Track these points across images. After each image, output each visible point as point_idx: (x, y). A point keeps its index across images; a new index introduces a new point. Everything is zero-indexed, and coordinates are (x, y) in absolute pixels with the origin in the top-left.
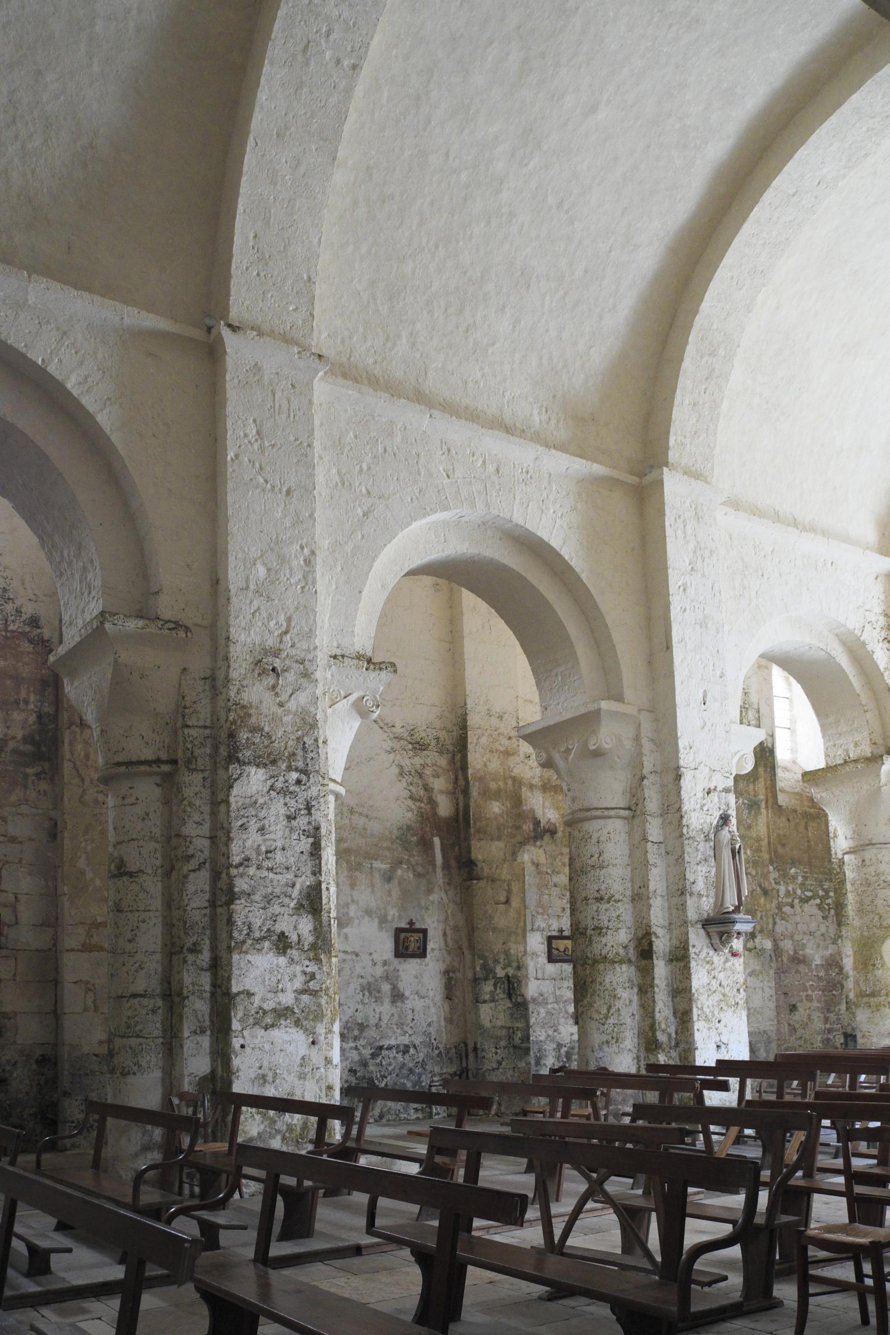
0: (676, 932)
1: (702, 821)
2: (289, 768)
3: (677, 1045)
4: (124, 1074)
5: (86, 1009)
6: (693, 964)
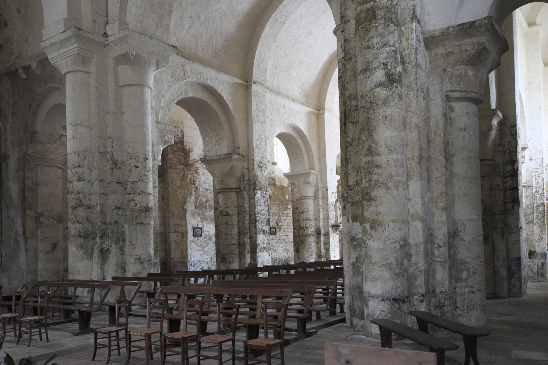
0: (326, 228)
2: (264, 191)
3: (325, 256)
5: (175, 249)
6: (330, 236)
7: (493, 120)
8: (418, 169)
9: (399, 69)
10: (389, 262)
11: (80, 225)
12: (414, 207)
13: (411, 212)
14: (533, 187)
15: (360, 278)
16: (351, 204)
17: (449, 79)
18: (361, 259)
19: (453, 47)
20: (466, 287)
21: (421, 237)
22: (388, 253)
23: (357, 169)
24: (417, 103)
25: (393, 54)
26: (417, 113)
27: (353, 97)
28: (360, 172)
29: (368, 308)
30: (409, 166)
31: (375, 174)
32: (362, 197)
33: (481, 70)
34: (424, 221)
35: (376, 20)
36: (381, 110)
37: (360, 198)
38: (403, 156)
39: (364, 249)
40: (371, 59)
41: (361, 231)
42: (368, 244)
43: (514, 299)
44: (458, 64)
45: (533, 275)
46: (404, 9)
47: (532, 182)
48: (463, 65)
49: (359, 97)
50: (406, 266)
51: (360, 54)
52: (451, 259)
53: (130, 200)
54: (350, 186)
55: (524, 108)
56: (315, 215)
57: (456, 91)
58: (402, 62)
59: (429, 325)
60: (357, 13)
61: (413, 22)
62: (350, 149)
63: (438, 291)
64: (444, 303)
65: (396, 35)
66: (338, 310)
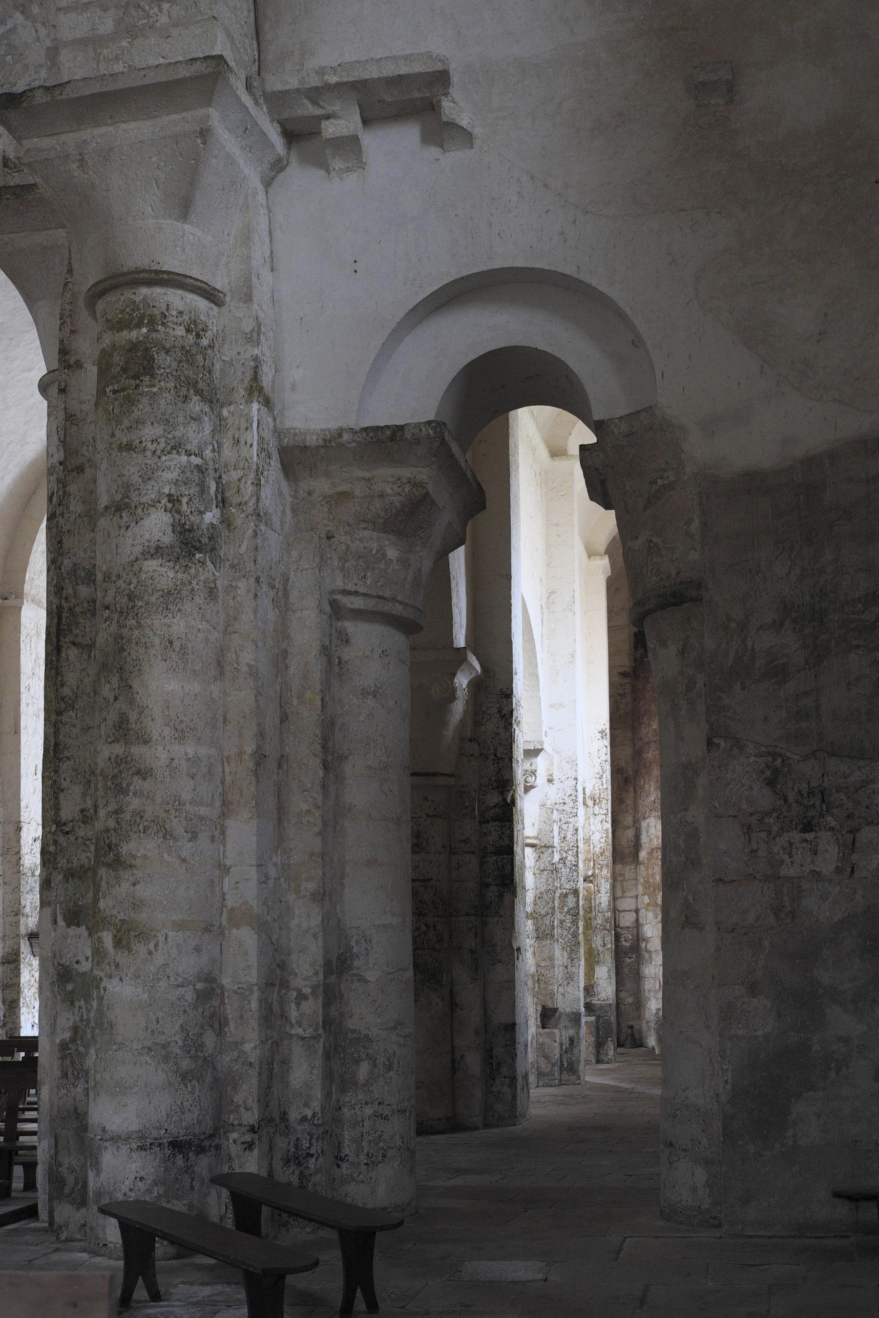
0: (9, 942)
1: (31, 861)
6: (22, 966)
7: (459, 675)
8: (253, 789)
9: (211, 517)
10: (162, 1039)
12: (237, 888)
13: (230, 903)
14: (555, 849)
15: (80, 1089)
16: (65, 875)
17: (340, 559)
18: (85, 1032)
19: (351, 483)
20: (366, 1103)
21: (254, 972)
22: (160, 1014)
23: (87, 776)
24: (255, 612)
25: (196, 475)
26: (253, 640)
27: (83, 574)
28: (93, 786)
29: (98, 1172)
30: (228, 779)
31: (135, 794)
32: (96, 857)
33: (418, 549)
34: (263, 928)
35: (152, 376)
36: (157, 621)
37: (90, 860)
38: (213, 751)
39: (95, 1004)
40: (136, 479)
41: (89, 953)
42: (105, 990)
43: (496, 1131)
44: (363, 525)
45: (549, 1069)
46: (231, 363)
47: (551, 835)
48: (373, 530)
49: (99, 577)
50: (210, 1051)
51: (105, 460)
52: (330, 1030)
54: (65, 824)
55: (535, 654)
57: (356, 593)
58: (220, 498)
59: (265, 1211)
60: (104, 349)
61: (252, 401)
62: (68, 720)
63: (294, 1116)
64: (309, 1148)
65: (208, 428)
66: (18, 1183)
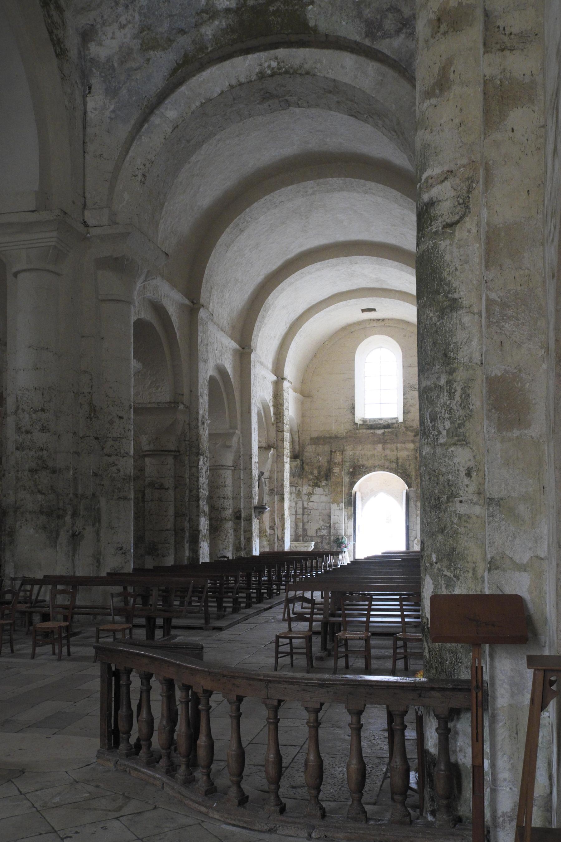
3: (245, 549)
4: (163, 556)
11: (43, 496)
53: (111, 465)
56: (233, 492)
